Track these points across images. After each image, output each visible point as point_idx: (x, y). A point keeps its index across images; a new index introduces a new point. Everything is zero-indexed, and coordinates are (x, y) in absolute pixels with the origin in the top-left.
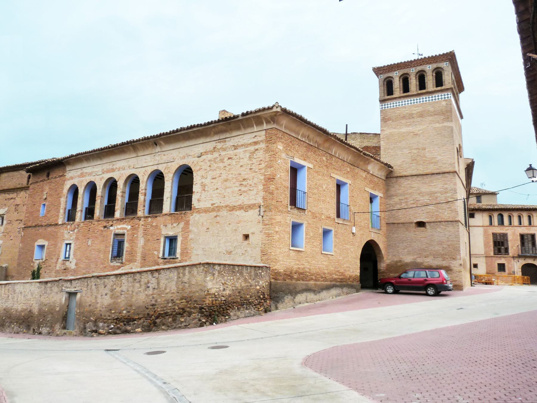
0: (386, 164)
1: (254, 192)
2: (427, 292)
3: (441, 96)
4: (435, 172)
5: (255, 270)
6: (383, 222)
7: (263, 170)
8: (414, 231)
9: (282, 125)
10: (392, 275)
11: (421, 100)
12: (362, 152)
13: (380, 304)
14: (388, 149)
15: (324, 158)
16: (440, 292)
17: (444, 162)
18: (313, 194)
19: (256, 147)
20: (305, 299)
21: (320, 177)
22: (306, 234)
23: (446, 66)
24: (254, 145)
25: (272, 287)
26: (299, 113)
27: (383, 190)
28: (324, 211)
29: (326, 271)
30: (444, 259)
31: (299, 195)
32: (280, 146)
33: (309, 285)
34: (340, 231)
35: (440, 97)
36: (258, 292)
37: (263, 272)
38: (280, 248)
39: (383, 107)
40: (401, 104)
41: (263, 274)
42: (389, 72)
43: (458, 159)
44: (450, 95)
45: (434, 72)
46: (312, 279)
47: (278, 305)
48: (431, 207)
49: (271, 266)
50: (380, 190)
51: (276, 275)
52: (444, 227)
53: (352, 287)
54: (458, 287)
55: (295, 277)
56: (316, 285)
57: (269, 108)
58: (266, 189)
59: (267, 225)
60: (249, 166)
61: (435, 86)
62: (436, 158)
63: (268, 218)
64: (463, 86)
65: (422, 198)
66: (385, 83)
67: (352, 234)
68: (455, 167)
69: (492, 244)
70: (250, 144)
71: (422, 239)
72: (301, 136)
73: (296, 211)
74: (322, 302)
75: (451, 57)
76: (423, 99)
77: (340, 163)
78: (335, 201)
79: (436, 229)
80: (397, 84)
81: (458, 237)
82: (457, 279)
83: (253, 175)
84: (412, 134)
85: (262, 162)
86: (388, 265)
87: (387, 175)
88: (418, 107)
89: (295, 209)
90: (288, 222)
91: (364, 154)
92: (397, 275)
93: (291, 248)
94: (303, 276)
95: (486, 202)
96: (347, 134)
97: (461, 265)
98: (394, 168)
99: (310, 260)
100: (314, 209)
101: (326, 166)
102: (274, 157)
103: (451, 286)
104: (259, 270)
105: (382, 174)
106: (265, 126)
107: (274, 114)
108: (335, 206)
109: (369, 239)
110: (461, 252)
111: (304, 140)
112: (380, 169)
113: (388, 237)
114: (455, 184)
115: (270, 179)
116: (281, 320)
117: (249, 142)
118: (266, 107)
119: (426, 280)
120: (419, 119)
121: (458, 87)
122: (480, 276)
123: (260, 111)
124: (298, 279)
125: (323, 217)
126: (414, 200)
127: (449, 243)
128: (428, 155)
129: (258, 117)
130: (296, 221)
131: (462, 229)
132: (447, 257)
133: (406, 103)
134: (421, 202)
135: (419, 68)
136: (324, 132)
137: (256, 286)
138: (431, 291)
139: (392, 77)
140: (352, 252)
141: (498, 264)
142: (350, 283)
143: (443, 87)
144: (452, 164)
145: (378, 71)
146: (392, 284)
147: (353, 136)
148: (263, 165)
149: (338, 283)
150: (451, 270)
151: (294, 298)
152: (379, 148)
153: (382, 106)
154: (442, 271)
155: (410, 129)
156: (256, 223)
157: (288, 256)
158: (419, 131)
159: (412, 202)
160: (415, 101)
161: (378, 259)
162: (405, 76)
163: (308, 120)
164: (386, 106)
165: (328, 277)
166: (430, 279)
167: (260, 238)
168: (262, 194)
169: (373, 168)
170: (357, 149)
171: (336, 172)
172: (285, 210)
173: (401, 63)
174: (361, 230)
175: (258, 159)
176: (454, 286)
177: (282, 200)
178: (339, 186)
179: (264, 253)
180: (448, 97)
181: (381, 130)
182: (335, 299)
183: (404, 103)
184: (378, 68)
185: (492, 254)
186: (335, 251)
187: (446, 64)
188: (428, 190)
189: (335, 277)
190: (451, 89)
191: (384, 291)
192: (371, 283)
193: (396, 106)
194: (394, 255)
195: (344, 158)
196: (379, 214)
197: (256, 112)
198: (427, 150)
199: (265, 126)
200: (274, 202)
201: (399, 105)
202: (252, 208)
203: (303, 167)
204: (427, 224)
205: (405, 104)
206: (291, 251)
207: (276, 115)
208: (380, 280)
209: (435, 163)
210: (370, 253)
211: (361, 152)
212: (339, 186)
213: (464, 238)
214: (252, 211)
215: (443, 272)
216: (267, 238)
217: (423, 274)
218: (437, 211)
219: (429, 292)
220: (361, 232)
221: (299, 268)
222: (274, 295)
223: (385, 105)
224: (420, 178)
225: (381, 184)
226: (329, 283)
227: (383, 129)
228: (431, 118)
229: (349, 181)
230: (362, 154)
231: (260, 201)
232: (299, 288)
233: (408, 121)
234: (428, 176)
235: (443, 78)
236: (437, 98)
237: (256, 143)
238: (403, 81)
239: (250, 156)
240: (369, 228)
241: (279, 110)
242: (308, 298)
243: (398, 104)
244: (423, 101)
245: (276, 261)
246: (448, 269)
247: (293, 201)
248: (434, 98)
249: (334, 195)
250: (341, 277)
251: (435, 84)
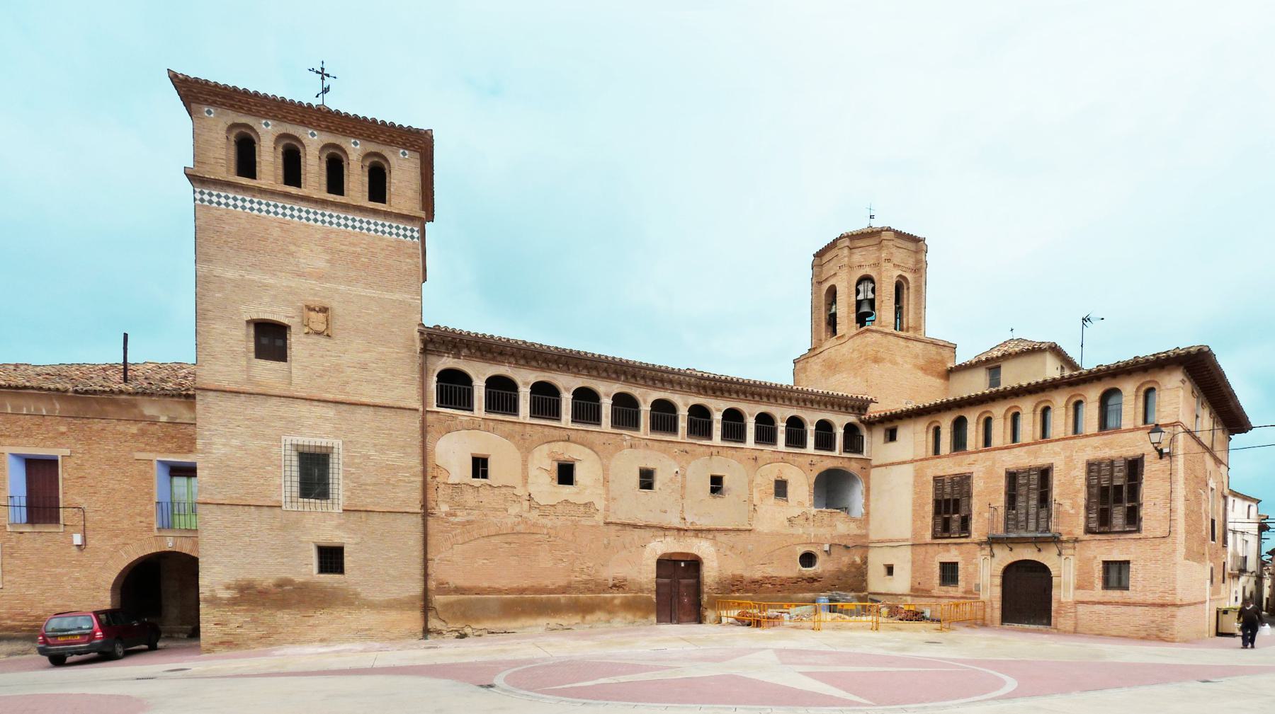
69: (930, 508)
185: (928, 536)
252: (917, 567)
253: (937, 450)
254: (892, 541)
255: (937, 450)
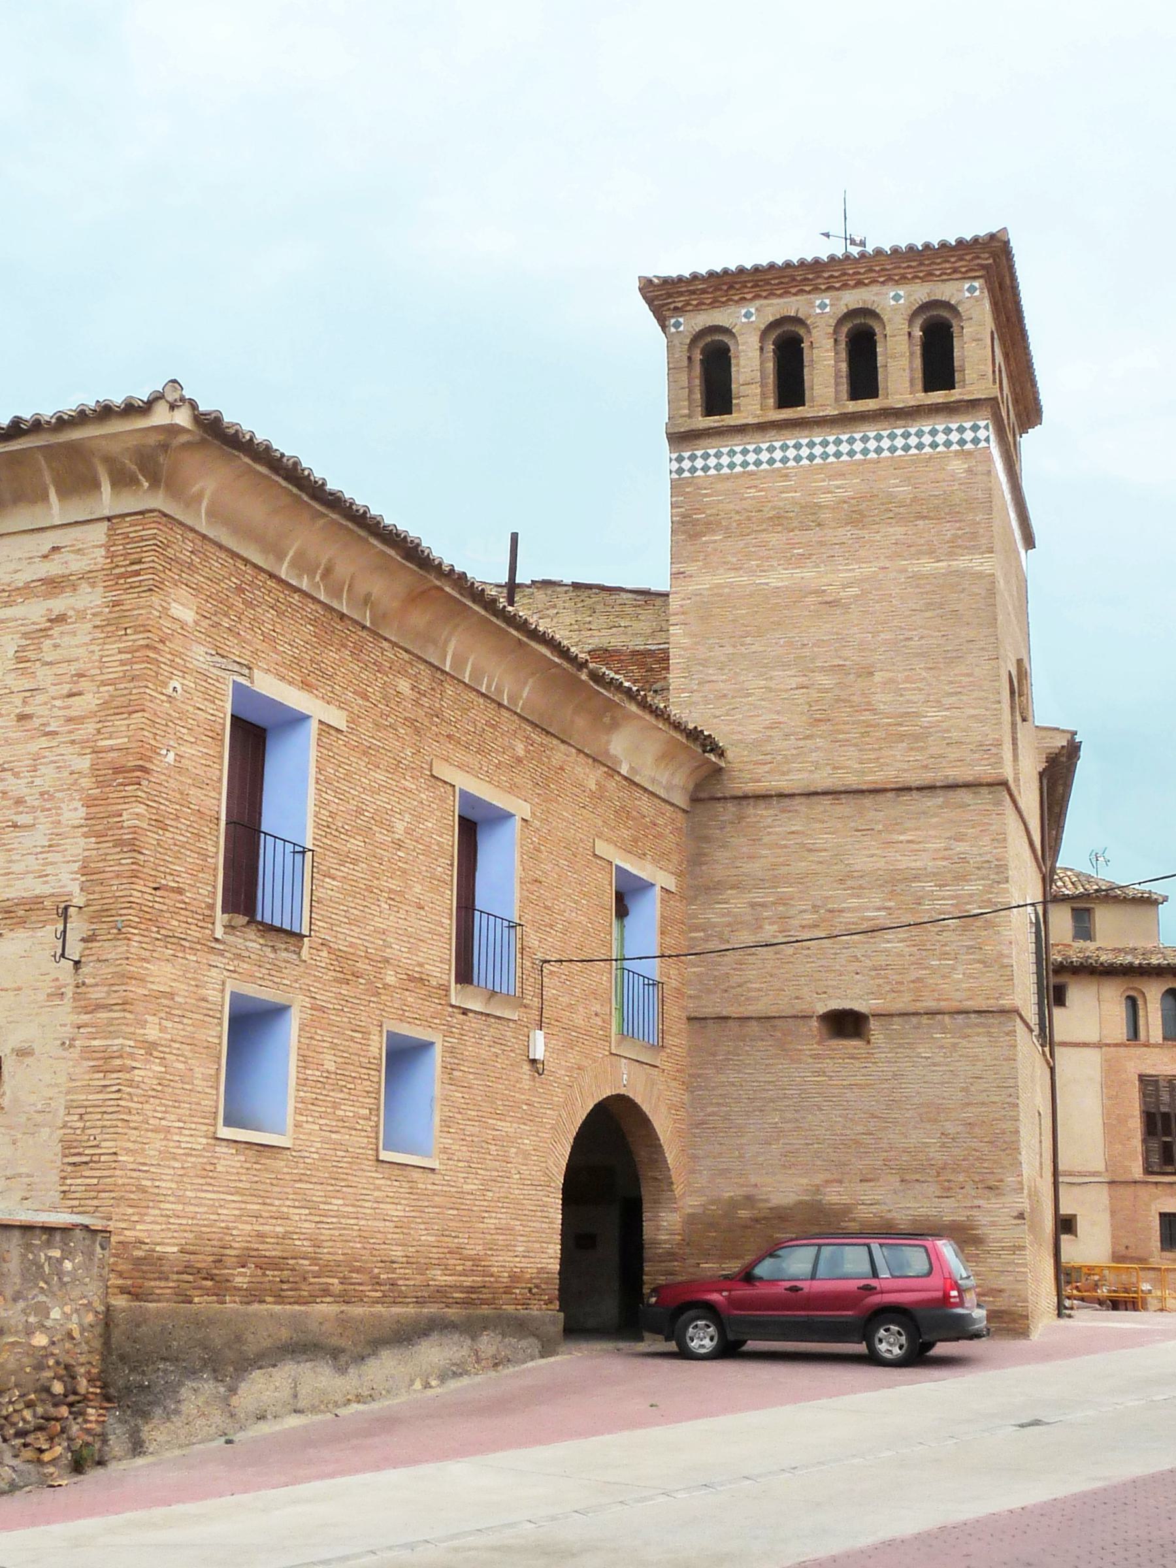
0: (694, 735)
1: (39, 838)
2: (871, 1346)
3: (948, 431)
4: (913, 779)
5: (28, 1247)
6: (674, 1012)
7: (90, 727)
8: (816, 1057)
9: (199, 498)
10: (710, 1268)
11: (858, 446)
12: (584, 665)
13: (658, 1413)
14: (704, 663)
15: (404, 686)
16: (931, 1345)
17: (955, 735)
18: (347, 858)
19: (58, 605)
20: (286, 1393)
21: (380, 776)
22: (303, 1059)
23: (970, 298)
24: (48, 596)
25: (117, 1335)
26: (284, 446)
27: (675, 858)
28: (397, 950)
29: (397, 1253)
30: (947, 1192)
31: (272, 860)
32: (184, 611)
33: (314, 1326)
34: (470, 1050)
35: (941, 438)
36: (40, 1367)
37: (68, 1254)
38: (167, 1130)
39: (686, 464)
40: (765, 456)
41: (68, 1265)
42: (715, 304)
43: (1014, 724)
44: (987, 433)
45: (919, 322)
46: (326, 1292)
47: (146, 1431)
48: (893, 943)
49: (112, 1225)
50: (660, 859)
51: (141, 1271)
52: (949, 1040)
53: (519, 1327)
54: (1010, 1323)
55: (240, 1281)
56: (343, 1321)
57: (131, 409)
58: (101, 823)
59: (99, 1007)
60: (17, 700)
61: (919, 384)
62: (917, 715)
63: (106, 970)
64: (1036, 401)
65: (854, 902)
66: (698, 356)
67: (526, 1067)
68: (1000, 761)
69: (1136, 1125)
70: (26, 591)
71: (849, 1095)
72: (293, 564)
73: (252, 942)
74: (375, 1406)
75: (991, 260)
76: (865, 439)
77: (481, 713)
78: (450, 897)
79: (911, 1046)
80: (751, 366)
81: (1009, 1086)
82: (1001, 1282)
83: (33, 747)
84: (811, 599)
85: (84, 684)
86: (691, 1220)
87: (698, 787)
88: (842, 475)
89: (251, 933)
90: (212, 995)
91: (597, 677)
92: (734, 1267)
93: (225, 1132)
94: (280, 1275)
95: (1113, 937)
96: (512, 587)
97: (1021, 1216)
98: (730, 755)
99: (317, 1194)
100: (346, 937)
101: (411, 722)
102: (148, 660)
103: (979, 1314)
104: (49, 1244)
105: (672, 781)
106: (108, 501)
107: (153, 440)
108: (449, 925)
109: (608, 1093)
110: (1024, 1158)
111: (305, 585)
112: (667, 757)
113: (693, 1083)
114: (1001, 839)
115: (126, 772)
116: (159, 1512)
117: (21, 579)
118: (118, 400)
119: (868, 1289)
120: (845, 533)
121: (1016, 402)
122: (1090, 1268)
123: (82, 417)
124: (253, 1295)
125: (390, 979)
126: (815, 908)
127: (969, 1114)
128: (883, 700)
129: (74, 450)
130: (250, 990)
131: (1027, 1046)
132: (961, 1178)
133: (791, 453)
134: (848, 917)
135: (852, 299)
136: (412, 553)
137: (29, 1333)
138: (890, 1343)
139: (726, 331)
140: (526, 1155)
141: (1162, 1215)
142: (510, 1308)
143: (955, 395)
144: (989, 749)
145: (665, 296)
146: (711, 1312)
147: (540, 595)
148: (89, 701)
149: (452, 1312)
150: (977, 1241)
151: (233, 1390)
152: (663, 658)
153: (680, 459)
154: (940, 1243)
155: (807, 575)
156: (42, 997)
157: (208, 1172)
158: (844, 587)
159: (809, 918)
160: (831, 449)
161: (646, 1193)
162: (788, 327)
163: (330, 486)
164: (699, 463)
165: (409, 1280)
166: (885, 1285)
167: (62, 1079)
168: (78, 846)
169: (633, 747)
170: (564, 653)
171: (459, 755)
172: (195, 933)
173: (772, 266)
174: (570, 1044)
175: (63, 668)
176: (993, 1316)
177: (185, 880)
178: (471, 829)
179: (77, 1157)
180: (976, 441)
181: (675, 575)
182: (437, 1390)
183: (778, 455)
184: (666, 281)
185: (1137, 1171)
186: (445, 1150)
187: (972, 289)
188: (881, 864)
189: (441, 1278)
190: (993, 403)
191: (672, 1346)
192: (609, 1307)
193: (745, 464)
194: (724, 1172)
195: (499, 691)
196: (653, 968)
197: (62, 423)
198: (878, 677)
199: (108, 501)
200: (140, 892)
201: (758, 463)
202: (22, 922)
203: (300, 719)
204: (873, 1024)
205: (785, 460)
206: (222, 1149)
207: (165, 447)
208: (656, 1290)
209: (916, 737)
210: (609, 1164)
211: (582, 672)
212: (471, 829)
213: (1035, 1097)
214: (21, 933)
215: (946, 1249)
216: (98, 1080)
217: (852, 1262)
218: (919, 965)
219: (883, 1347)
220: (573, 1057)
221: (261, 1236)
222: (124, 1376)
223: (693, 458)
224: (845, 808)
225: (668, 823)
226: (411, 1310)
227: (681, 567)
228: (897, 531)
229: (519, 808)
230: (584, 677)
231: (66, 881)
232: (258, 1340)
233: (798, 536)
234: (880, 798)
235: (957, 353)
236: (927, 439)
237: (54, 585)
238: (769, 353)
239: (22, 649)
240: (607, 1038)
241: (182, 418)
242: (303, 1391)
243: (751, 458)
244: (865, 452)
245: (142, 1198)
246: (966, 1237)
247: (242, 891)
248: (913, 441)
249: (447, 867)
250: (468, 1281)
251: (919, 375)
252: (1120, 1221)
253: (1134, 1033)
254: (1081, 1174)
255: (1134, 1033)
